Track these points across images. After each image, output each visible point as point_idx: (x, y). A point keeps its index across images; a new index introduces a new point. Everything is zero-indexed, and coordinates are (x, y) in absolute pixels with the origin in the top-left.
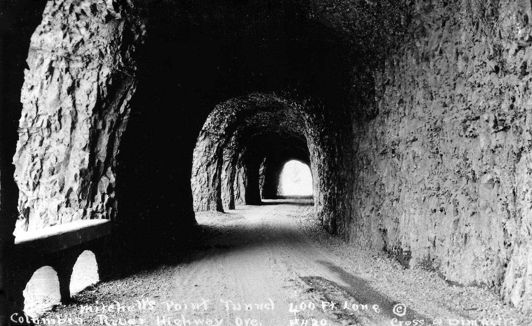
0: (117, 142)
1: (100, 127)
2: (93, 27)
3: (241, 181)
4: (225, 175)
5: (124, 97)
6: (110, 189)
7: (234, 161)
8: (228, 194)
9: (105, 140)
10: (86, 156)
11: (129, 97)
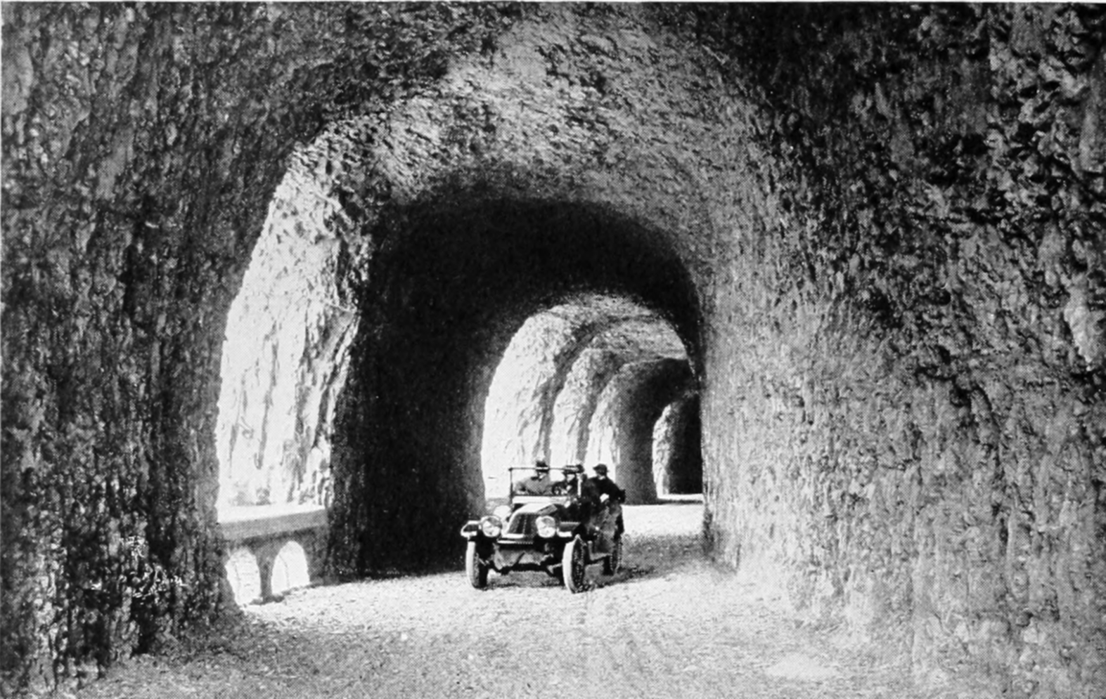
1: (308, 383)
5: (342, 339)
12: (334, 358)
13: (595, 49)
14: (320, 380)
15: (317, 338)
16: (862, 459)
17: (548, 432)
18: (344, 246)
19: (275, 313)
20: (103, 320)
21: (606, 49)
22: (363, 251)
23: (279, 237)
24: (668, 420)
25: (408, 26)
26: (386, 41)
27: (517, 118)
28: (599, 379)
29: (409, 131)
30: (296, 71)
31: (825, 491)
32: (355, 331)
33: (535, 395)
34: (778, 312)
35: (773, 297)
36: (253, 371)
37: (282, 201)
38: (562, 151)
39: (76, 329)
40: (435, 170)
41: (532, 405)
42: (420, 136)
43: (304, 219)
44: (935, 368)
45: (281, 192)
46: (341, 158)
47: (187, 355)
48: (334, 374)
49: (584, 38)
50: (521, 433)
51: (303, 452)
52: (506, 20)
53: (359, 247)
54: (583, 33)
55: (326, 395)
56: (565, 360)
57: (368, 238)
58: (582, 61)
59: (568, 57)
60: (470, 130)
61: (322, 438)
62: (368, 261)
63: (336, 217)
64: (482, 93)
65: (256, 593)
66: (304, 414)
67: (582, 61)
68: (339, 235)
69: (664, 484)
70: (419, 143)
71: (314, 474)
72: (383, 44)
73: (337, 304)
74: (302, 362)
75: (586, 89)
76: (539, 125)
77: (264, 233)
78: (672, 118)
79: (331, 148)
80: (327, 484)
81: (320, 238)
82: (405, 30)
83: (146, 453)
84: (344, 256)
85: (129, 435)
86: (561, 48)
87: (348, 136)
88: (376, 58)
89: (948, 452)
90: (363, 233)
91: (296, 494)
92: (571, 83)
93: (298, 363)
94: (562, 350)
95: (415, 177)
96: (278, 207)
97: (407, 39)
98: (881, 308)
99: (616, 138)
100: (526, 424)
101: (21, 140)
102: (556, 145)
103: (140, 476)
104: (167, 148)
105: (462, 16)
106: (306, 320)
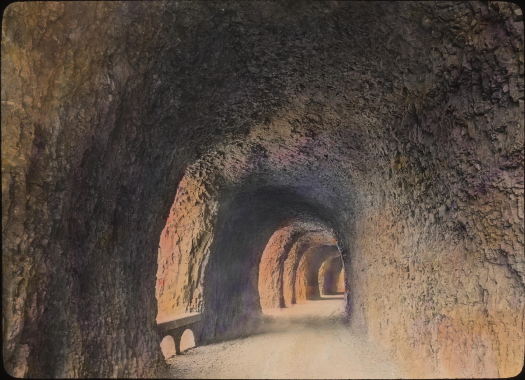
1: (194, 262)
2: (189, 208)
4: (287, 280)
5: (206, 244)
10: (187, 278)
12: (203, 252)
13: (312, 121)
14: (198, 261)
15: (196, 244)
16: (448, 299)
17: (282, 274)
18: (207, 206)
19: (179, 234)
20: (102, 244)
21: (317, 120)
22: (214, 208)
23: (180, 203)
24: (323, 268)
25: (235, 111)
26: (225, 118)
27: (277, 152)
28: (300, 253)
29: (233, 158)
30: (188, 131)
31: (423, 310)
32: (212, 241)
33: (277, 261)
34: (393, 230)
35: (390, 224)
36: (171, 258)
37: (182, 188)
38: (295, 166)
39: (88, 248)
40: (243, 174)
41: (275, 265)
42: (237, 160)
43: (191, 195)
44: (496, 259)
45: (182, 184)
46: (205, 170)
47: (143, 255)
48: (204, 258)
49: (308, 116)
50: (272, 276)
51: (192, 291)
52: (276, 109)
53: (213, 206)
54: (308, 113)
55: (200, 267)
56: (288, 248)
57: (217, 202)
58: (306, 126)
59: (301, 124)
60: (258, 157)
61: (199, 284)
62: (216, 212)
63: (204, 194)
64: (263, 141)
65: (174, 351)
66: (192, 274)
67: (306, 126)
68: (205, 201)
69: (322, 292)
70: (237, 163)
71: (196, 299)
72: (224, 120)
73: (205, 230)
74: (190, 253)
75: (307, 138)
76: (286, 154)
77: (175, 201)
78: (344, 149)
79: (201, 166)
80: (201, 303)
81: (197, 203)
82: (234, 113)
83: (124, 303)
84: (207, 211)
85: (116, 296)
86: (298, 120)
87: (208, 161)
88: (221, 126)
89: (504, 300)
90: (215, 200)
91: (189, 308)
92: (301, 136)
93: (189, 254)
94: (287, 243)
95: (235, 177)
96: (180, 191)
97: (234, 117)
98: (461, 229)
99: (318, 159)
100: (274, 272)
101: (54, 156)
102: (292, 163)
103: (121, 314)
104: (131, 164)
105: (258, 106)
106: (192, 236)
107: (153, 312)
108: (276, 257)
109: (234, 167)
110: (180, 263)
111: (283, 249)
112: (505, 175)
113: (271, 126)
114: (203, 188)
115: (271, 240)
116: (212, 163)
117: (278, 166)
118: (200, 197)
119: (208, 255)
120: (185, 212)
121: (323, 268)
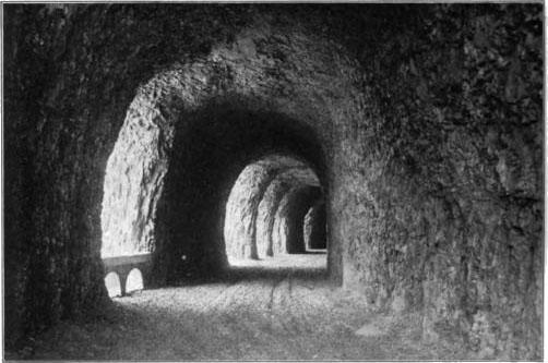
0: (155, 205)
1: (144, 194)
2: (140, 133)
3: (282, 231)
4: (261, 226)
5: (160, 175)
6: (151, 233)
7: (273, 211)
8: (276, 239)
9: (147, 201)
10: (136, 212)
11: (163, 176)
18: (162, 132)
24: (311, 215)
28: (279, 196)
41: (247, 206)
45: (133, 105)
55: (152, 201)
56: (263, 187)
63: (158, 117)
79: (156, 86)
90: (171, 125)
92: (268, 57)
107: (179, 8)
108: (248, 198)
109: (194, 88)
110: (128, 195)
111: (257, 188)
112: (437, 111)
113: (234, 45)
114: (158, 111)
115: (242, 176)
116: (168, 83)
117: (245, 89)
118: (154, 121)
119: (161, 188)
120: (135, 138)
121: (311, 215)
